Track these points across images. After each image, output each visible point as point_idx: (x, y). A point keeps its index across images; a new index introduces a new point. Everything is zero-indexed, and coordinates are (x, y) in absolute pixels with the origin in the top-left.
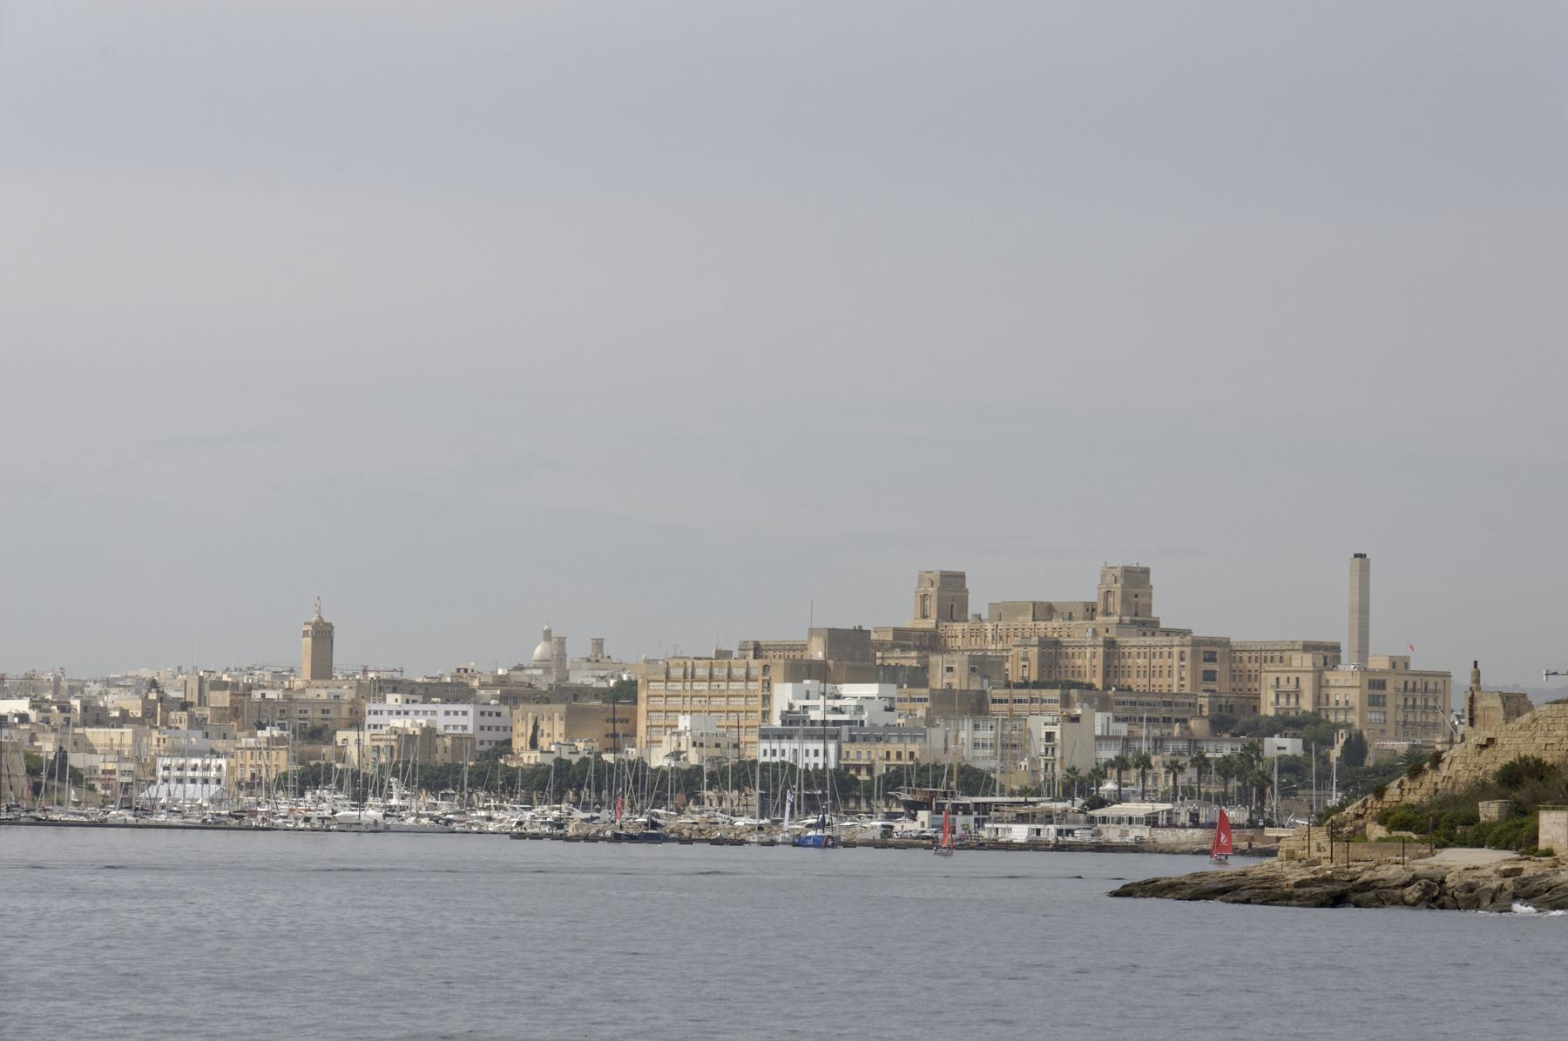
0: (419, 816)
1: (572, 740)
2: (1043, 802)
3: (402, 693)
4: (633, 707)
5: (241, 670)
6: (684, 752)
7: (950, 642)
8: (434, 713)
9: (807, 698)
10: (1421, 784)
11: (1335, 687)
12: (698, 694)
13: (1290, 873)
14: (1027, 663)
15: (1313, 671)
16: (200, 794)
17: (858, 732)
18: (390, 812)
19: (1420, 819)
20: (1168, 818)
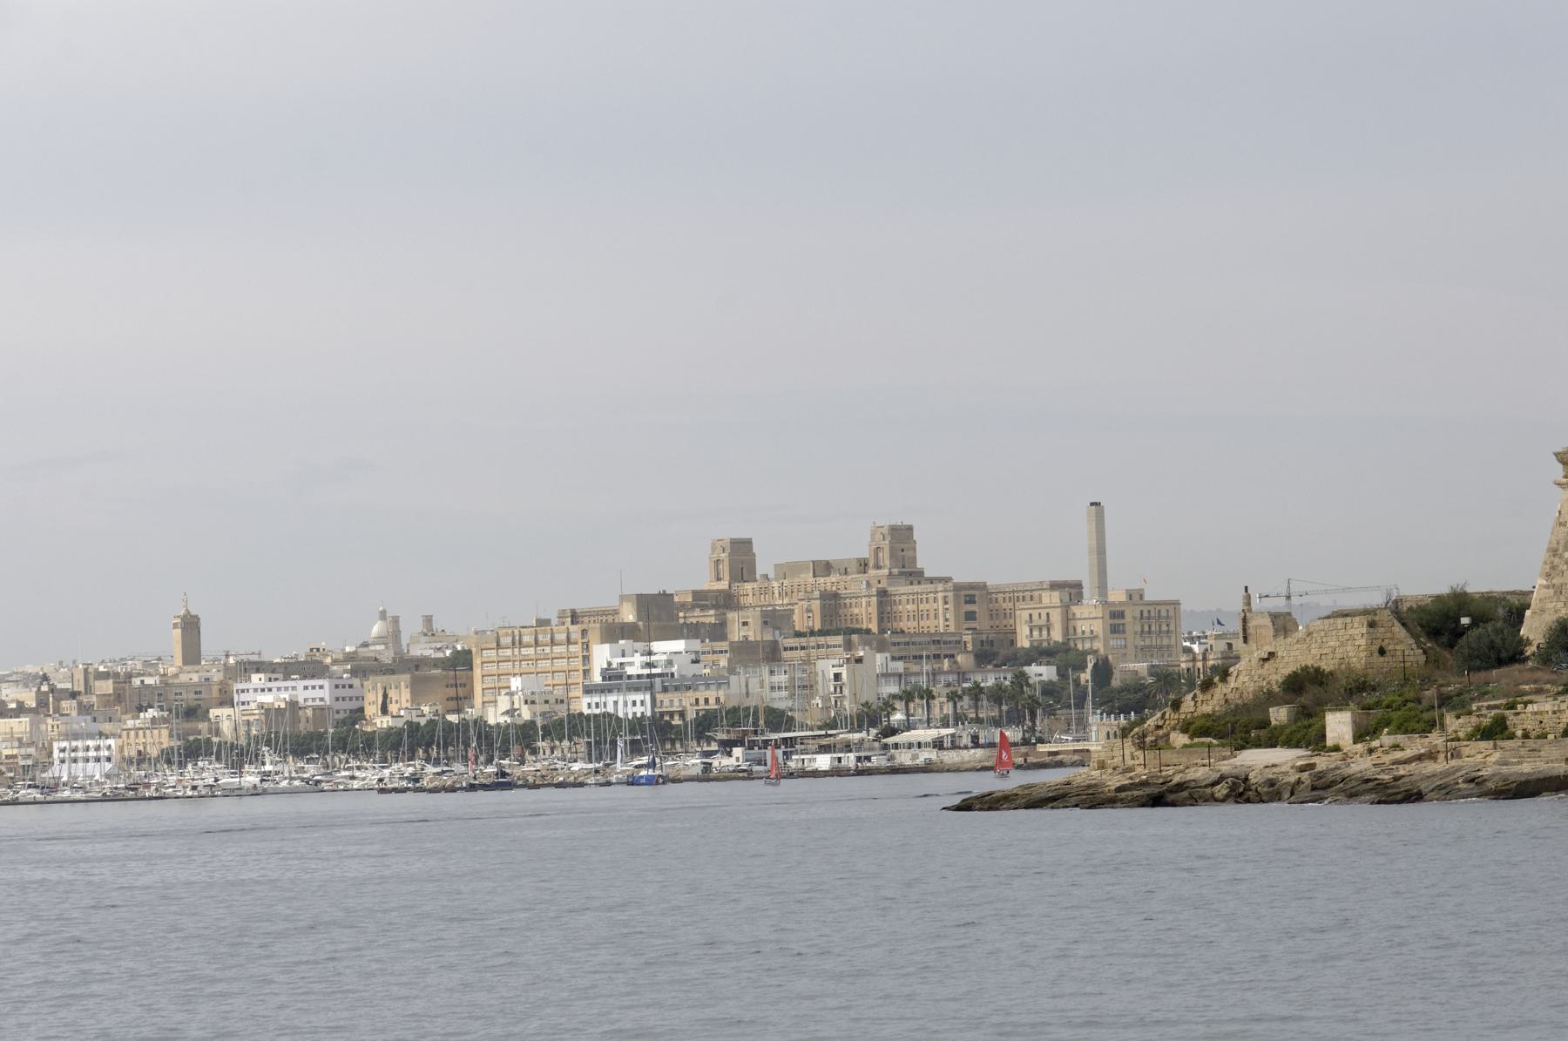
0: (292, 779)
1: (419, 704)
2: (842, 733)
3: (265, 673)
4: (469, 673)
5: (115, 662)
6: (517, 710)
8: (294, 688)
9: (623, 656)
10: (1212, 696)
11: (1080, 619)
12: (526, 658)
13: (1110, 780)
14: (810, 614)
15: (1061, 607)
16: (96, 771)
17: (670, 683)
18: (265, 776)
19: (1217, 726)
20: (952, 741)
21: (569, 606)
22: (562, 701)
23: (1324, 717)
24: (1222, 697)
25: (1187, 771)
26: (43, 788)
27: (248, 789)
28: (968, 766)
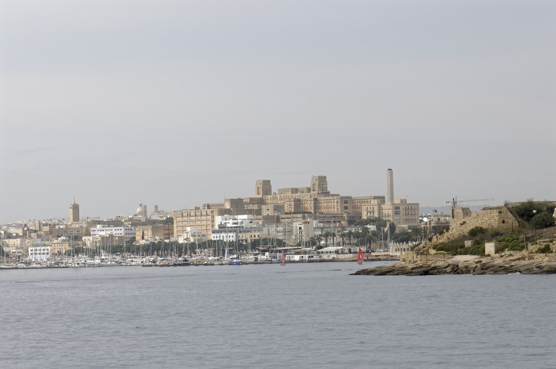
0: (112, 261)
1: (155, 236)
2: (303, 248)
4: (172, 225)
7: (267, 201)
8: (111, 230)
9: (226, 220)
10: (443, 236)
11: (384, 209)
15: (378, 205)
18: (102, 260)
20: (342, 251)
21: (207, 203)
22: (204, 236)
23: (484, 244)
24: (447, 236)
25: (436, 263)
26: (26, 263)
27: (97, 264)
28: (347, 260)
